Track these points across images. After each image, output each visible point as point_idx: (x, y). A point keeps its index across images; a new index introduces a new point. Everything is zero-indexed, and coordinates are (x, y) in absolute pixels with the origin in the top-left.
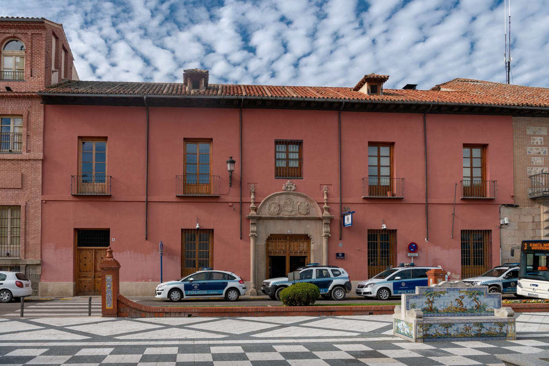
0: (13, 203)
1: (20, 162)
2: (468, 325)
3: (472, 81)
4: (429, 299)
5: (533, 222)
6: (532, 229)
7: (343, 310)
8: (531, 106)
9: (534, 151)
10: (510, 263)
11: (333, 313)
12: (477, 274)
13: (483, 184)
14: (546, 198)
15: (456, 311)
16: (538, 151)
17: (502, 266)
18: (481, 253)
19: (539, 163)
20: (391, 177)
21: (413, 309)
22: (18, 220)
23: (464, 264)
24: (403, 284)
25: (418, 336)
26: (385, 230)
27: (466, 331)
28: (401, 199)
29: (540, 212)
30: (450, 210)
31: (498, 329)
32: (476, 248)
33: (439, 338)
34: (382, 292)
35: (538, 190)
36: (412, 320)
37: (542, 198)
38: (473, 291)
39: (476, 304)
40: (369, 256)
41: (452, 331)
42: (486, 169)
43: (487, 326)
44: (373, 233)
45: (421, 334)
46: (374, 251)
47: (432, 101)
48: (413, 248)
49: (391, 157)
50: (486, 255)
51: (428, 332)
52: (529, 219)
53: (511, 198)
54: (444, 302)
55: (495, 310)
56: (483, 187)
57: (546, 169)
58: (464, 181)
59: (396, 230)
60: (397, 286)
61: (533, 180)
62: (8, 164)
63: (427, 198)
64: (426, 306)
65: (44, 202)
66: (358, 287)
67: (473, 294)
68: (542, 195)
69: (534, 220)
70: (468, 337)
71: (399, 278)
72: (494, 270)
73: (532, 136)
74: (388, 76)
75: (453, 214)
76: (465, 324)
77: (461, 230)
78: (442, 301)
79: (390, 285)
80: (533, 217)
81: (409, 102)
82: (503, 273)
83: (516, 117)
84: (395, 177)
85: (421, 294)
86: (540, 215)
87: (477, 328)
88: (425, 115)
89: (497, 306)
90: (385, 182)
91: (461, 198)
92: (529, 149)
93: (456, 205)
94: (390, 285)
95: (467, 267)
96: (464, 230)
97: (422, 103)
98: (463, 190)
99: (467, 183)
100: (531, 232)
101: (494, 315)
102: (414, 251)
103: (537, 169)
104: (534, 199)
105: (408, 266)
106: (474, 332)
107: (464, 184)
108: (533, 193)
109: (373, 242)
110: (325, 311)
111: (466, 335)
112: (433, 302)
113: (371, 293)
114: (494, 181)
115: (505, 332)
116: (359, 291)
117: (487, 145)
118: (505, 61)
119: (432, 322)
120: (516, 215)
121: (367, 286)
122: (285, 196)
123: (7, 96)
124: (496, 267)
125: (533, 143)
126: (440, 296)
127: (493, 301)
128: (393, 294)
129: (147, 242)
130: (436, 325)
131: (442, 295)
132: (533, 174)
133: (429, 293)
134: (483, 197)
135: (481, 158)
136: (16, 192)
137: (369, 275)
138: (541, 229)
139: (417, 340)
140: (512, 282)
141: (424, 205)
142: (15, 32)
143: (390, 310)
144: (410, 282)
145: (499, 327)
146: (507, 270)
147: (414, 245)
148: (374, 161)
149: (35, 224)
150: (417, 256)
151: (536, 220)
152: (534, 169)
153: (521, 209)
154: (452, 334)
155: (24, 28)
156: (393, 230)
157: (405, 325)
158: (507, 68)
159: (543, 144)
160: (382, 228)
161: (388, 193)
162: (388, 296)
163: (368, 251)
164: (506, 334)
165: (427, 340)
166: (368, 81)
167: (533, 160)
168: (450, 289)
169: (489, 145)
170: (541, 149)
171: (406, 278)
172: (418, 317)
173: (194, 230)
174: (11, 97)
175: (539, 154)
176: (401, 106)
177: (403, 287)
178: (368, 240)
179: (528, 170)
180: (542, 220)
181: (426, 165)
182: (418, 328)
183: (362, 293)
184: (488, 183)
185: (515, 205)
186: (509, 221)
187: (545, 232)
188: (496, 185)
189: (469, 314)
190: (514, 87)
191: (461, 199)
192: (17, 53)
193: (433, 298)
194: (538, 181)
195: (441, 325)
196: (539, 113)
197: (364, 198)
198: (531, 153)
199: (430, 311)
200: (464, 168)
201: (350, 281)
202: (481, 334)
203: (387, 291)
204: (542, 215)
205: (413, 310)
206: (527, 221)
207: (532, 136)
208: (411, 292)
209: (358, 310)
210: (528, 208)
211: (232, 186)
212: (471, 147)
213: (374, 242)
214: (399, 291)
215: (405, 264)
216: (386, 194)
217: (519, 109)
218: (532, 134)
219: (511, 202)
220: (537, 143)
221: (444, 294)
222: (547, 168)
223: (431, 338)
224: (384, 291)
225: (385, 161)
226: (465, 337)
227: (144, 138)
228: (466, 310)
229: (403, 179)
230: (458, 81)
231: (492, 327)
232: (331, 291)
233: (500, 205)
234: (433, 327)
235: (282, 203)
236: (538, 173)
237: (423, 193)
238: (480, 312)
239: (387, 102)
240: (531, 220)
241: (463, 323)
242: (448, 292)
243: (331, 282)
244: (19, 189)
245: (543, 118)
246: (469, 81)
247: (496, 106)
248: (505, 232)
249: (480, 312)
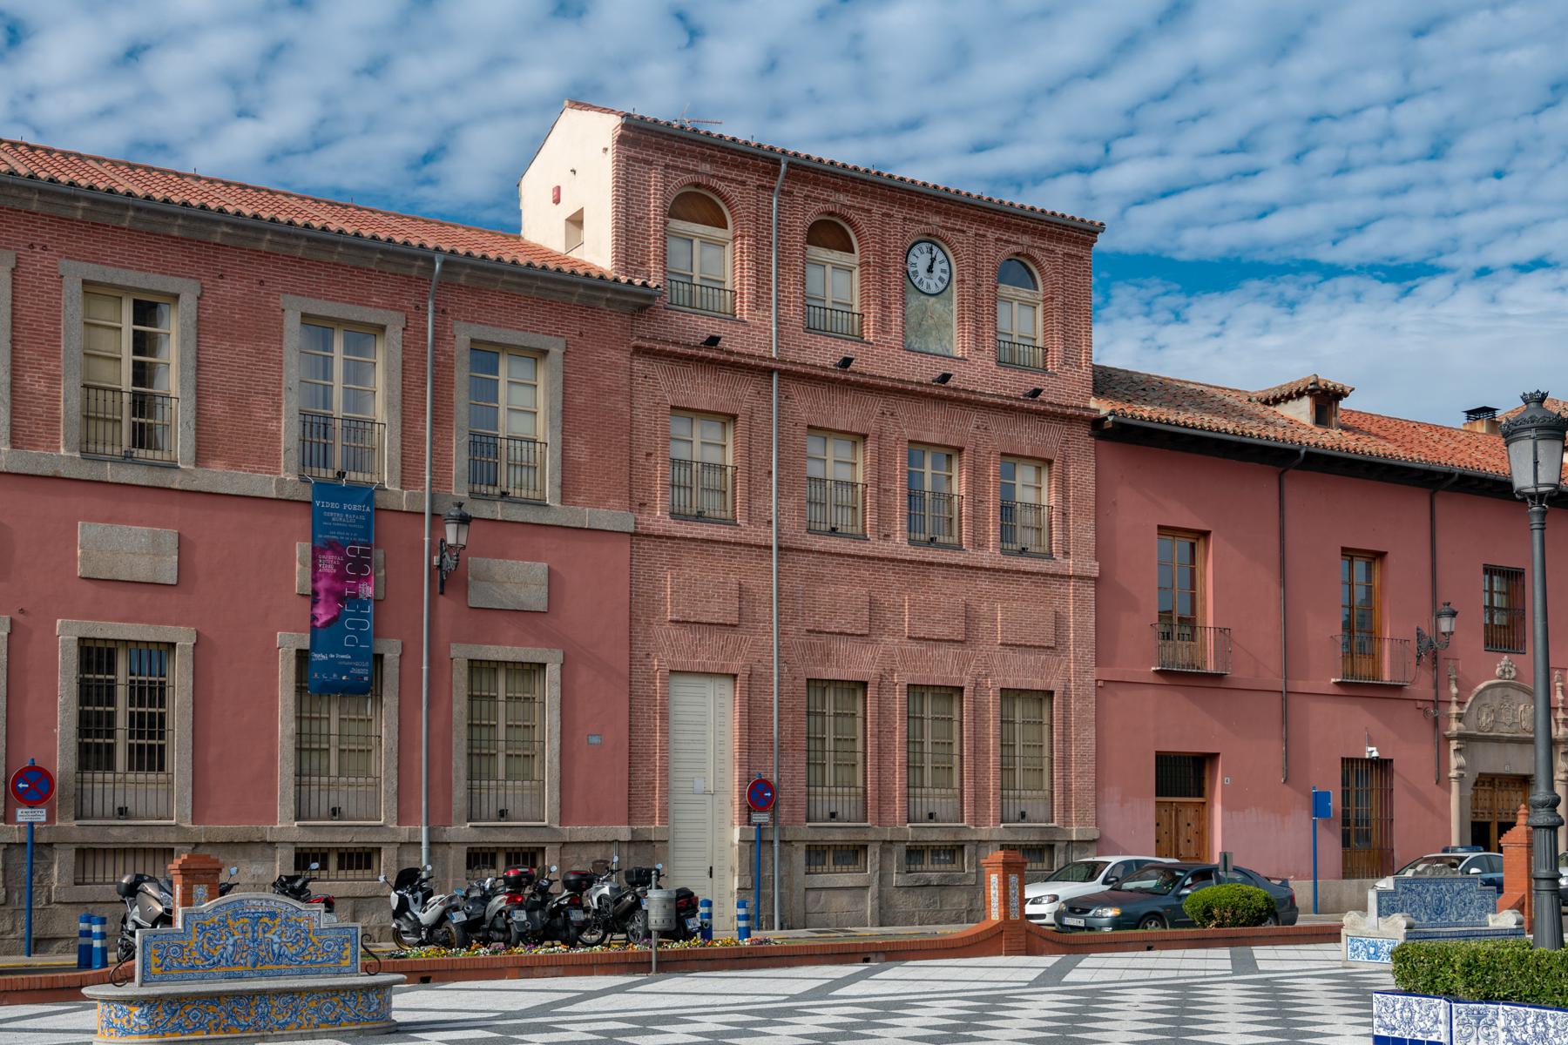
0: (1038, 684)
1: (1050, 580)
12: (1363, 873)
22: (819, 719)
26: (1372, 761)
62: (1026, 583)
65: (1103, 686)
88: (1435, 492)
117: (1385, 553)
122: (1499, 689)
123: (702, 359)
129: (1287, 789)
136: (1043, 657)
141: (1278, 696)
142: (1030, 243)
149: (1084, 740)
155: (1051, 238)
160: (1367, 756)
169: (1389, 555)
173: (1363, 760)
174: (1038, 413)
192: (1026, 295)
197: (1156, 671)
211: (446, 591)
227: (1274, 540)
235: (1496, 704)
244: (1048, 648)
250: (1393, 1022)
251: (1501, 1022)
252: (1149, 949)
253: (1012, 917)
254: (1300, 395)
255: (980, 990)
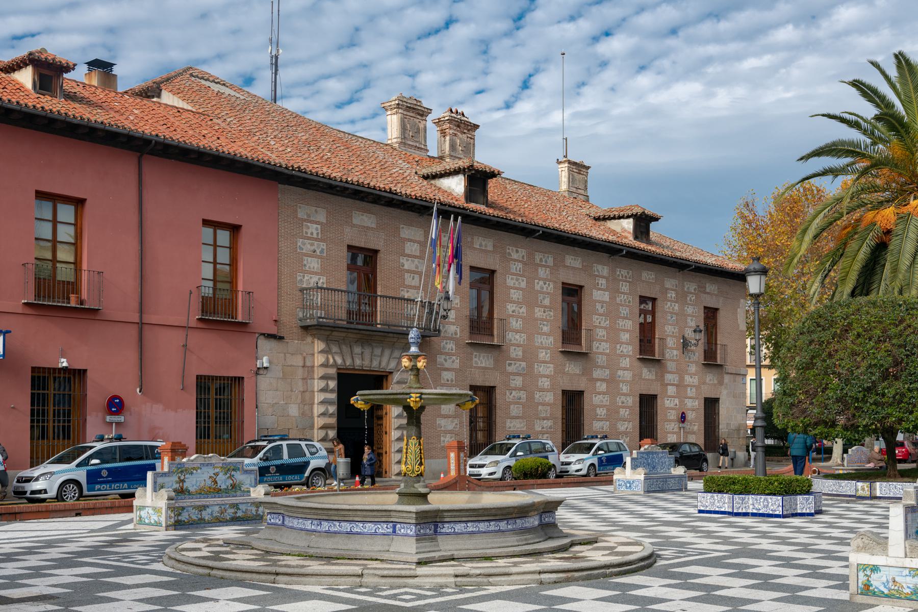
2: (223, 507)
3: (216, 81)
4: (179, 478)
5: (303, 367)
6: (302, 377)
7: (35, 510)
8: (305, 172)
9: (308, 247)
10: (269, 434)
11: (18, 516)
13: (232, 295)
14: (322, 328)
15: (210, 492)
16: (312, 248)
17: (258, 441)
18: (228, 419)
19: (314, 268)
20: (77, 263)
21: (162, 490)
23: (201, 438)
24: (104, 473)
25: (169, 522)
26: (65, 369)
27: (221, 514)
28: (95, 311)
29: (314, 351)
30: (179, 336)
31: (254, 509)
32: (220, 409)
33: (192, 524)
34: (65, 491)
35: (311, 313)
36: (162, 503)
37: (317, 327)
38: (229, 467)
39: (232, 482)
40: (32, 421)
41: (206, 515)
42: (237, 269)
43: (242, 507)
44: (41, 375)
45: (172, 520)
46: (43, 410)
47: (153, 133)
48: (115, 405)
49: (78, 225)
50: (235, 421)
51: (180, 518)
52: (298, 361)
53: (273, 323)
54: (197, 481)
55: (252, 489)
56: (232, 299)
57: (323, 279)
58: (203, 288)
59: (85, 371)
60: (93, 477)
61: (305, 296)
63: (141, 312)
64: (176, 486)
66: (18, 481)
67: (228, 470)
68: (316, 324)
69: (304, 363)
70: (224, 522)
71: (97, 461)
72: (246, 447)
73: (305, 220)
74: (75, 65)
75: (185, 346)
76: (220, 505)
77: (197, 376)
78: (195, 480)
79: (81, 475)
80: (304, 358)
81: (114, 128)
82: (260, 452)
83: (283, 186)
84: (85, 266)
85: (171, 471)
86: (313, 355)
87: (233, 510)
88: (141, 156)
89: (253, 484)
90: (65, 273)
91: (197, 317)
92: (300, 242)
93: (189, 329)
94: (81, 475)
95: (204, 442)
96: (201, 376)
97: (137, 135)
98: (200, 304)
99: (209, 292)
100: (300, 383)
101: (250, 496)
102: (117, 413)
103: (311, 278)
104: (306, 328)
105: (111, 440)
106: (229, 515)
107: (203, 291)
108: (304, 319)
109: (41, 392)
110: (4, 514)
111: (221, 519)
112: (185, 481)
113: (45, 491)
114: (249, 292)
115: (262, 514)
116: (20, 490)
118: (271, 53)
119: (185, 505)
120: (279, 353)
121: (37, 479)
124: (250, 442)
125: (306, 233)
126: (192, 473)
127: (249, 478)
128: (85, 492)
130: (189, 508)
131: (195, 472)
132: (304, 286)
133: (180, 470)
134: (232, 318)
135: (230, 248)
137: (32, 458)
138: (314, 379)
139: (167, 528)
140: (272, 466)
141: (136, 326)
143: (107, 508)
144: (116, 468)
145: (256, 509)
146: (265, 446)
147: (118, 401)
148: (45, 231)
150: (123, 421)
151: (308, 364)
152: (306, 278)
153: (287, 343)
154: (206, 518)
156: (80, 370)
157: (151, 511)
158: (274, 66)
159: (320, 237)
160: (60, 366)
161: (73, 297)
162: (77, 495)
163: (31, 410)
164: (262, 516)
165: (179, 527)
166: (35, 65)
167: (305, 262)
168: (203, 464)
169: (87, 201)
170: (317, 244)
171: (108, 462)
172: (170, 499)
175: (314, 252)
176: (100, 133)
177: (104, 478)
178: (33, 387)
179: (299, 278)
180: (316, 364)
181: (142, 251)
182: (169, 512)
183: (29, 493)
184: (240, 295)
185: (279, 336)
186: (270, 362)
187: (319, 384)
188: (251, 299)
189: (224, 494)
190: (283, 112)
191: (197, 319)
193: (184, 476)
194: (312, 298)
195: (195, 507)
196: (315, 185)
197: (25, 304)
198: (303, 249)
199: (181, 492)
200: (203, 263)
201: (5, 470)
202: (237, 518)
203: (75, 487)
204: (316, 355)
205: (163, 491)
206: (295, 364)
207: (305, 220)
208: (117, 487)
209: (58, 509)
210: (298, 343)
212: (215, 226)
213: (39, 392)
214: (97, 486)
215: (106, 437)
216: (68, 298)
217: (287, 175)
218: (305, 217)
219: (273, 330)
220: (312, 234)
221: (197, 471)
222: (325, 278)
223: (183, 525)
224: (70, 486)
225: (66, 233)
226: (221, 522)
228: (221, 490)
229: (99, 273)
230: (191, 75)
231: (249, 508)
232: (308, 478)
233: (257, 335)
234: (185, 511)
236: (311, 285)
237: (135, 305)
238: (235, 492)
239: (75, 121)
240: (301, 364)
241: (218, 505)
242: (201, 468)
243: (307, 464)
245: (320, 193)
246: (211, 79)
247: (254, 163)
248: (264, 382)
249: (235, 492)
250: (760, 507)
251: (751, 502)
252: (514, 489)
253: (461, 474)
254: (628, 217)
255: (61, 535)
